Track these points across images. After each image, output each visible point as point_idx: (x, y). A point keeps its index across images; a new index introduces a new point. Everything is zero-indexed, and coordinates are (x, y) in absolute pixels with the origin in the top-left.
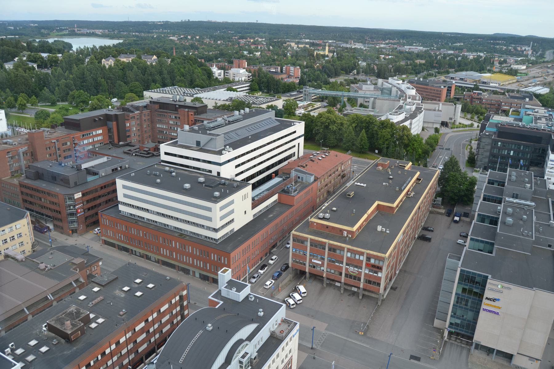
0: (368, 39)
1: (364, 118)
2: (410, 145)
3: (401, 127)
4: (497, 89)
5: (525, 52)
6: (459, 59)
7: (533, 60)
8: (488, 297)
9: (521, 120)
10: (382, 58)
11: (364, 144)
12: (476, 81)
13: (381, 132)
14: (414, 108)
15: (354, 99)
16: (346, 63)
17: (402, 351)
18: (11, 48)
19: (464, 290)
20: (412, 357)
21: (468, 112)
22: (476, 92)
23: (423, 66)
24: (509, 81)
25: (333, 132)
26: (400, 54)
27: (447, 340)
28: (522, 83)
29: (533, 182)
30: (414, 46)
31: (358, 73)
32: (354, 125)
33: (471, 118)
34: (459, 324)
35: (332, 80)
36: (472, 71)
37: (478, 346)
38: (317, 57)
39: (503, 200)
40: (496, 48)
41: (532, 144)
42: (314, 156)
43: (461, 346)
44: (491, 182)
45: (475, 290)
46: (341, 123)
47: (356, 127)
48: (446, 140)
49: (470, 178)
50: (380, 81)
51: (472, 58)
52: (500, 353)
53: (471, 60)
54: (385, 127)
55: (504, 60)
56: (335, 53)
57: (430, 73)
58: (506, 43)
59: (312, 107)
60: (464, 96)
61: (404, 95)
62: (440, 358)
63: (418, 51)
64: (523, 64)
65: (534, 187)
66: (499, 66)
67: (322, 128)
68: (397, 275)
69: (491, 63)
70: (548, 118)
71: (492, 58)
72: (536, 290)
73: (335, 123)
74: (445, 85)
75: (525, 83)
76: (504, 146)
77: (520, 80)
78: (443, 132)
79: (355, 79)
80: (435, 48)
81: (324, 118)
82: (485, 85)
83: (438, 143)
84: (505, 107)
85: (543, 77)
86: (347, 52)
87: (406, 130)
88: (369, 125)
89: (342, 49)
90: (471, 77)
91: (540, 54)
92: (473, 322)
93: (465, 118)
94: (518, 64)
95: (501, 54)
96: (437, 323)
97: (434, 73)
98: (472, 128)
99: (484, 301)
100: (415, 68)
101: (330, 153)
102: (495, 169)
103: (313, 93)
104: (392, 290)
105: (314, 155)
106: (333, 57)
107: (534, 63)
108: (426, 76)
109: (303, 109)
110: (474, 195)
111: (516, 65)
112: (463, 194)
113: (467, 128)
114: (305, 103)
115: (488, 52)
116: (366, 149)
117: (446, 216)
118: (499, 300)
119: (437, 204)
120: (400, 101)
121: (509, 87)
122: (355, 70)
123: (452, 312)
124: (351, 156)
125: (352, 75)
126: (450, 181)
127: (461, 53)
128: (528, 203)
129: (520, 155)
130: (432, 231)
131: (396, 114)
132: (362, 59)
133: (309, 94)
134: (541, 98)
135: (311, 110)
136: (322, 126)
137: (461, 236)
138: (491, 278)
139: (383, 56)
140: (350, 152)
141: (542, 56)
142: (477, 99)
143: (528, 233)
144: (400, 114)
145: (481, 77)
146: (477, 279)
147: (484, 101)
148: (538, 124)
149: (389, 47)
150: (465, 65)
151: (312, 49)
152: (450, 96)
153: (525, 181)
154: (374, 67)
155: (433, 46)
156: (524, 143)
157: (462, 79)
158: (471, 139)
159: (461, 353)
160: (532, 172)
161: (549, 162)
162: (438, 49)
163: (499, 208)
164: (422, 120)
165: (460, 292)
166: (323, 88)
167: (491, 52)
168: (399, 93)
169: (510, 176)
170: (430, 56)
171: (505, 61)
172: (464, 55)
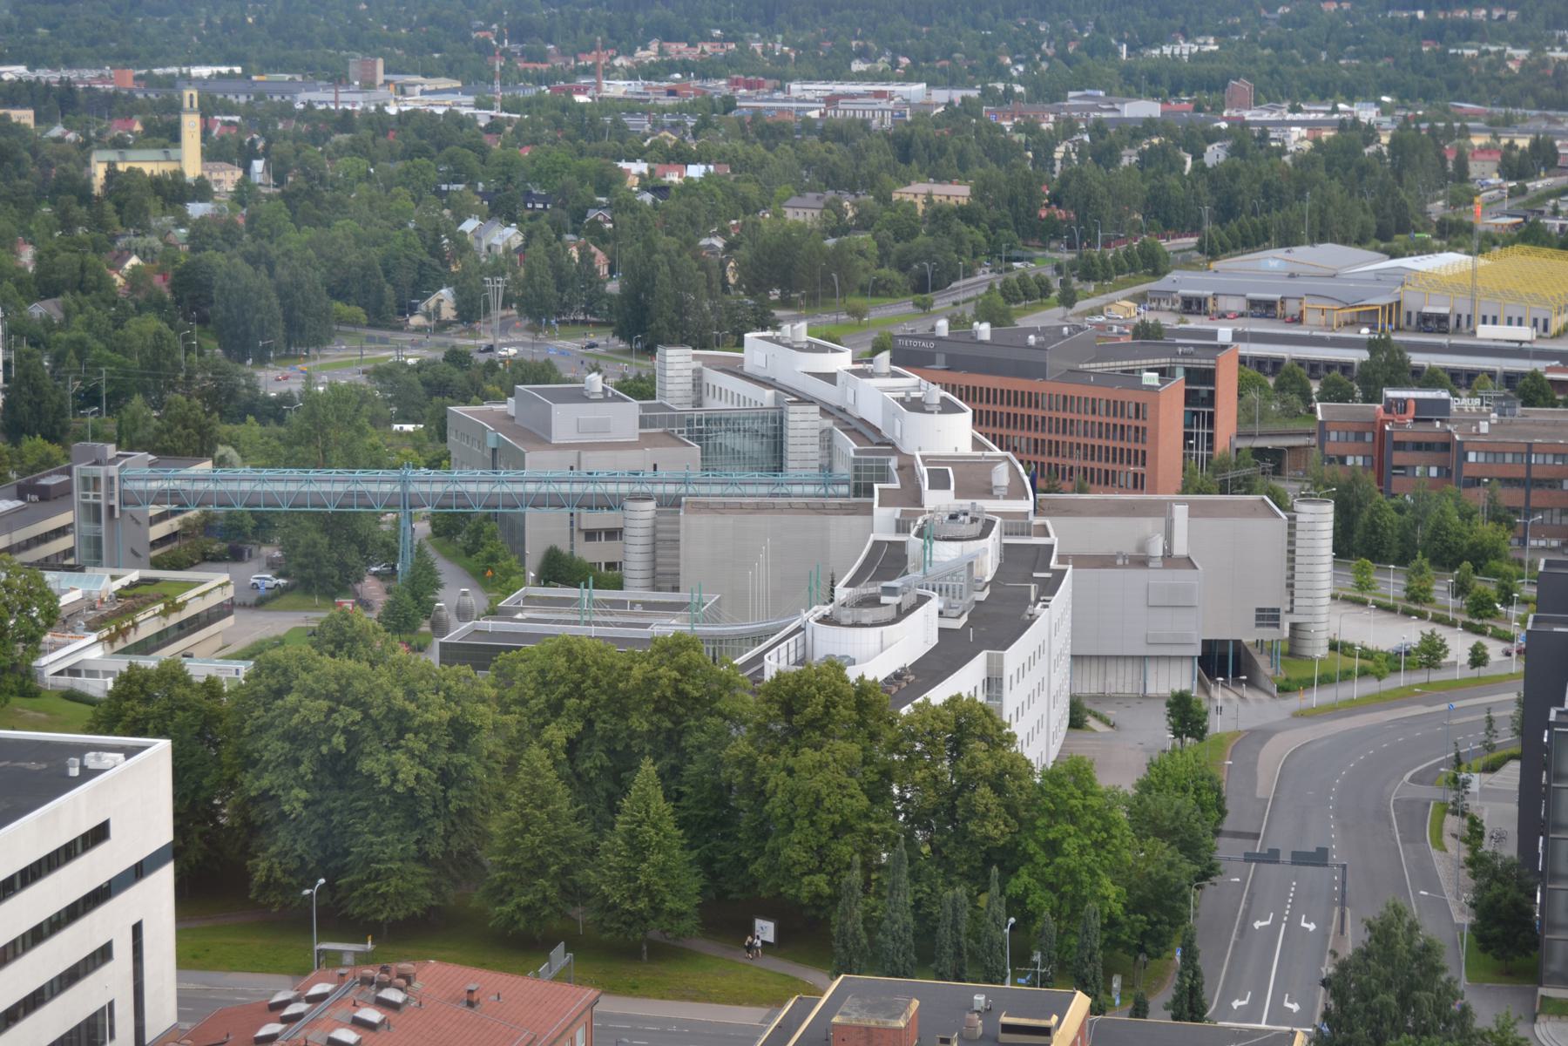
0: (500, 40)
1: (637, 672)
2: (1030, 858)
3: (936, 713)
4: (1540, 365)
6: (1214, 154)
10: (633, 183)
11: (659, 884)
12: (1368, 317)
13: (791, 772)
14: (987, 555)
15: (487, 517)
16: (359, 241)
18: (272, 190)
21: (1377, 553)
22: (1405, 401)
23: (964, 228)
25: (394, 806)
26: (769, 148)
30: (861, 77)
31: (470, 312)
32: (557, 733)
33: (1413, 598)
35: (274, 381)
36: (1322, 239)
38: (120, 207)
42: (285, 1020)
46: (453, 722)
47: (572, 746)
48: (1266, 785)
50: (677, 363)
51: (1307, 145)
53: (1303, 161)
54: (812, 724)
55: (1535, 145)
56: (258, 165)
57: (1023, 278)
58: (1524, 17)
59: (165, 614)
61: (894, 463)
63: (898, 116)
67: (300, 781)
69: (1447, 176)
71: (1449, 134)
73: (401, 733)
74: (1163, 362)
78: (1231, 727)
79: (457, 358)
80: (1019, 89)
81: (312, 694)
82: (1443, 340)
83: (1223, 813)
86: (355, 149)
87: (982, 737)
88: (678, 721)
89: (304, 128)
93: (1364, 603)
95: (1503, 103)
97: (1048, 272)
98: (1436, 676)
100: (900, 246)
101: (416, 985)
103: (160, 497)
105: (289, 1011)
106: (244, 194)
108: (1000, 302)
109: (93, 637)
113: (1402, 679)
114: (104, 583)
115: (1405, 95)
116: (681, 915)
120: (868, 510)
122: (446, 293)
124: (590, 993)
125: (419, 329)
127: (1217, 108)
131: (868, 614)
132: (484, 195)
133: (124, 503)
135: (159, 635)
136: (297, 762)
139: (639, 167)
140: (560, 956)
142: (1418, 446)
144: (901, 613)
145: (1402, 278)
147: (1472, 457)
149: (671, 92)
150: (1267, 196)
151: (59, 140)
152: (1211, 438)
154: (586, 257)
155: (1001, 73)
157: (1263, 309)
158: (1458, 761)
162: (1047, 92)
164: (1062, 645)
166: (222, 450)
167: (1427, 95)
168: (848, 446)
170: (998, 150)
172: (1245, 124)
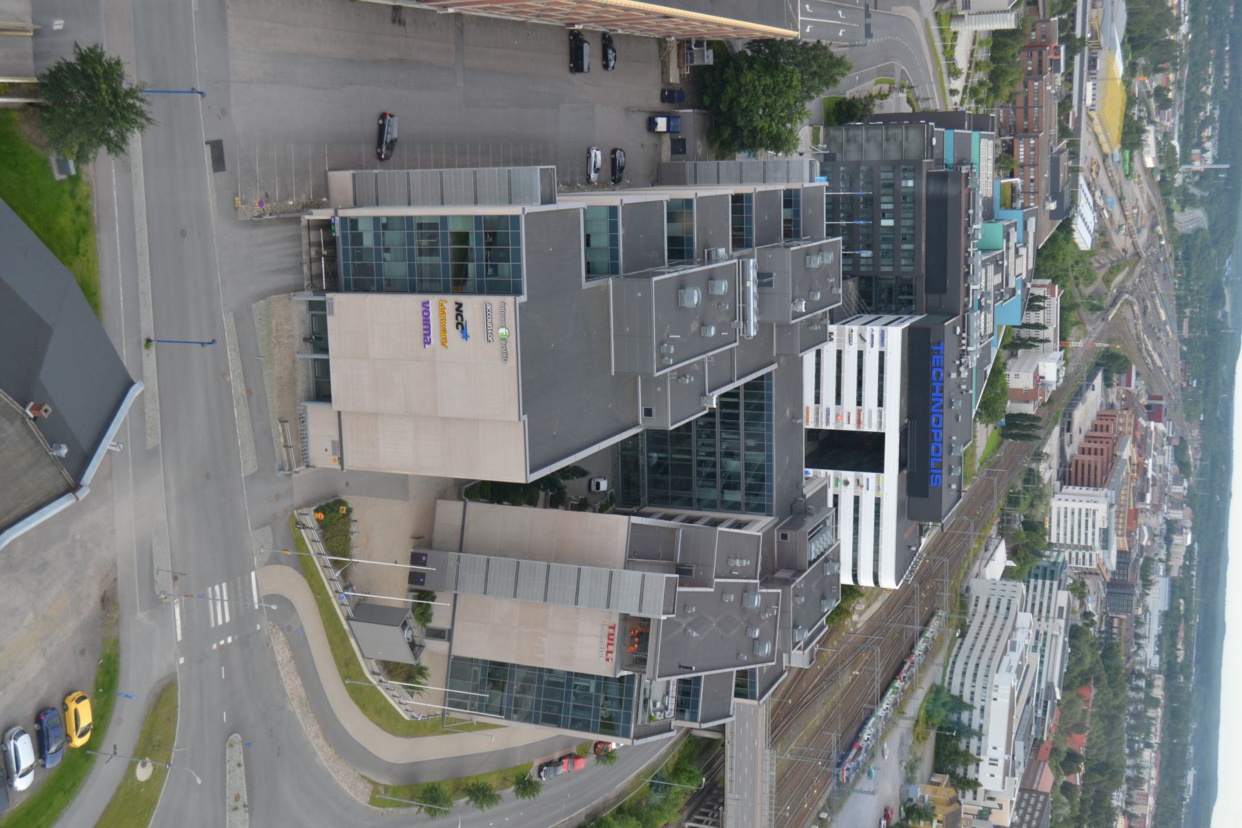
4: (1075, 109)
5: (1198, 151)
7: (1174, 180)
8: (463, 309)
9: (989, 217)
12: (1095, 36)
17: (224, 112)
19: (462, 237)
20: (217, 148)
22: (1059, 54)
24: (1105, 132)
27: (304, 223)
28: (1102, 172)
29: (815, 313)
33: (977, 64)
34: (362, 245)
37: (318, 312)
39: (746, 251)
40: (1206, 65)
41: (923, 271)
43: (302, 264)
44: (791, 199)
45: (472, 267)
49: (791, 131)
52: (323, 369)
55: (1170, 100)
60: (1047, 21)
62: (245, 221)
64: (1160, 157)
65: (802, 322)
66: (1148, 92)
68: (444, 12)
70: (1003, 290)
71: (1175, 64)
72: (522, 423)
75: (1103, 180)
76: (904, 198)
77: (1109, 161)
84: (1022, 150)
85: (1123, 221)
90: (1109, 19)
91: (1193, 195)
92: (380, 281)
93: (974, 44)
94: (1158, 143)
96: (341, 180)
98: (945, 76)
99: (450, 300)
102: (831, 216)
104: (390, 11)
107: (1164, 187)
110: (741, 157)
111: (1156, 138)
112: (741, 122)
113: (943, 62)
115: (1192, 44)
117: (663, 91)
118: (465, 336)
119: (692, 54)
121: (1085, 138)
123: (388, 218)
126: (773, 77)
128: (753, 319)
129: (884, 246)
130: (606, 67)
134: (1062, 236)
137: (614, 151)
138: (520, 304)
141: (1187, 201)
142: (1040, 61)
143: (670, 356)
145: (1112, 49)
146: (505, 268)
147: (1036, 84)
148: (984, 271)
153: (812, 293)
156: (923, 249)
158: (911, 88)
159: (282, 271)
160: (843, 291)
161: (877, 329)
163: (722, 251)
165: (455, 227)
167: (1192, 53)
169: (820, 249)
171: (1164, 104)
